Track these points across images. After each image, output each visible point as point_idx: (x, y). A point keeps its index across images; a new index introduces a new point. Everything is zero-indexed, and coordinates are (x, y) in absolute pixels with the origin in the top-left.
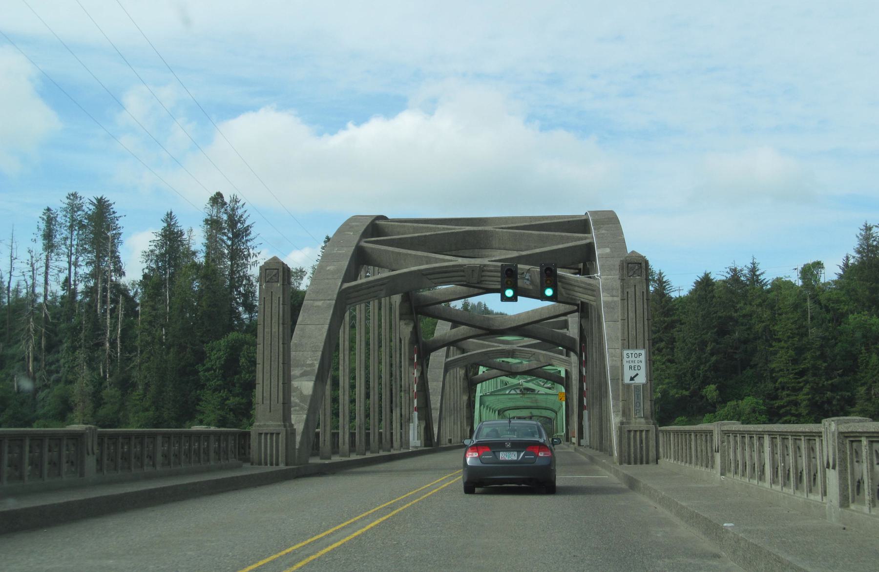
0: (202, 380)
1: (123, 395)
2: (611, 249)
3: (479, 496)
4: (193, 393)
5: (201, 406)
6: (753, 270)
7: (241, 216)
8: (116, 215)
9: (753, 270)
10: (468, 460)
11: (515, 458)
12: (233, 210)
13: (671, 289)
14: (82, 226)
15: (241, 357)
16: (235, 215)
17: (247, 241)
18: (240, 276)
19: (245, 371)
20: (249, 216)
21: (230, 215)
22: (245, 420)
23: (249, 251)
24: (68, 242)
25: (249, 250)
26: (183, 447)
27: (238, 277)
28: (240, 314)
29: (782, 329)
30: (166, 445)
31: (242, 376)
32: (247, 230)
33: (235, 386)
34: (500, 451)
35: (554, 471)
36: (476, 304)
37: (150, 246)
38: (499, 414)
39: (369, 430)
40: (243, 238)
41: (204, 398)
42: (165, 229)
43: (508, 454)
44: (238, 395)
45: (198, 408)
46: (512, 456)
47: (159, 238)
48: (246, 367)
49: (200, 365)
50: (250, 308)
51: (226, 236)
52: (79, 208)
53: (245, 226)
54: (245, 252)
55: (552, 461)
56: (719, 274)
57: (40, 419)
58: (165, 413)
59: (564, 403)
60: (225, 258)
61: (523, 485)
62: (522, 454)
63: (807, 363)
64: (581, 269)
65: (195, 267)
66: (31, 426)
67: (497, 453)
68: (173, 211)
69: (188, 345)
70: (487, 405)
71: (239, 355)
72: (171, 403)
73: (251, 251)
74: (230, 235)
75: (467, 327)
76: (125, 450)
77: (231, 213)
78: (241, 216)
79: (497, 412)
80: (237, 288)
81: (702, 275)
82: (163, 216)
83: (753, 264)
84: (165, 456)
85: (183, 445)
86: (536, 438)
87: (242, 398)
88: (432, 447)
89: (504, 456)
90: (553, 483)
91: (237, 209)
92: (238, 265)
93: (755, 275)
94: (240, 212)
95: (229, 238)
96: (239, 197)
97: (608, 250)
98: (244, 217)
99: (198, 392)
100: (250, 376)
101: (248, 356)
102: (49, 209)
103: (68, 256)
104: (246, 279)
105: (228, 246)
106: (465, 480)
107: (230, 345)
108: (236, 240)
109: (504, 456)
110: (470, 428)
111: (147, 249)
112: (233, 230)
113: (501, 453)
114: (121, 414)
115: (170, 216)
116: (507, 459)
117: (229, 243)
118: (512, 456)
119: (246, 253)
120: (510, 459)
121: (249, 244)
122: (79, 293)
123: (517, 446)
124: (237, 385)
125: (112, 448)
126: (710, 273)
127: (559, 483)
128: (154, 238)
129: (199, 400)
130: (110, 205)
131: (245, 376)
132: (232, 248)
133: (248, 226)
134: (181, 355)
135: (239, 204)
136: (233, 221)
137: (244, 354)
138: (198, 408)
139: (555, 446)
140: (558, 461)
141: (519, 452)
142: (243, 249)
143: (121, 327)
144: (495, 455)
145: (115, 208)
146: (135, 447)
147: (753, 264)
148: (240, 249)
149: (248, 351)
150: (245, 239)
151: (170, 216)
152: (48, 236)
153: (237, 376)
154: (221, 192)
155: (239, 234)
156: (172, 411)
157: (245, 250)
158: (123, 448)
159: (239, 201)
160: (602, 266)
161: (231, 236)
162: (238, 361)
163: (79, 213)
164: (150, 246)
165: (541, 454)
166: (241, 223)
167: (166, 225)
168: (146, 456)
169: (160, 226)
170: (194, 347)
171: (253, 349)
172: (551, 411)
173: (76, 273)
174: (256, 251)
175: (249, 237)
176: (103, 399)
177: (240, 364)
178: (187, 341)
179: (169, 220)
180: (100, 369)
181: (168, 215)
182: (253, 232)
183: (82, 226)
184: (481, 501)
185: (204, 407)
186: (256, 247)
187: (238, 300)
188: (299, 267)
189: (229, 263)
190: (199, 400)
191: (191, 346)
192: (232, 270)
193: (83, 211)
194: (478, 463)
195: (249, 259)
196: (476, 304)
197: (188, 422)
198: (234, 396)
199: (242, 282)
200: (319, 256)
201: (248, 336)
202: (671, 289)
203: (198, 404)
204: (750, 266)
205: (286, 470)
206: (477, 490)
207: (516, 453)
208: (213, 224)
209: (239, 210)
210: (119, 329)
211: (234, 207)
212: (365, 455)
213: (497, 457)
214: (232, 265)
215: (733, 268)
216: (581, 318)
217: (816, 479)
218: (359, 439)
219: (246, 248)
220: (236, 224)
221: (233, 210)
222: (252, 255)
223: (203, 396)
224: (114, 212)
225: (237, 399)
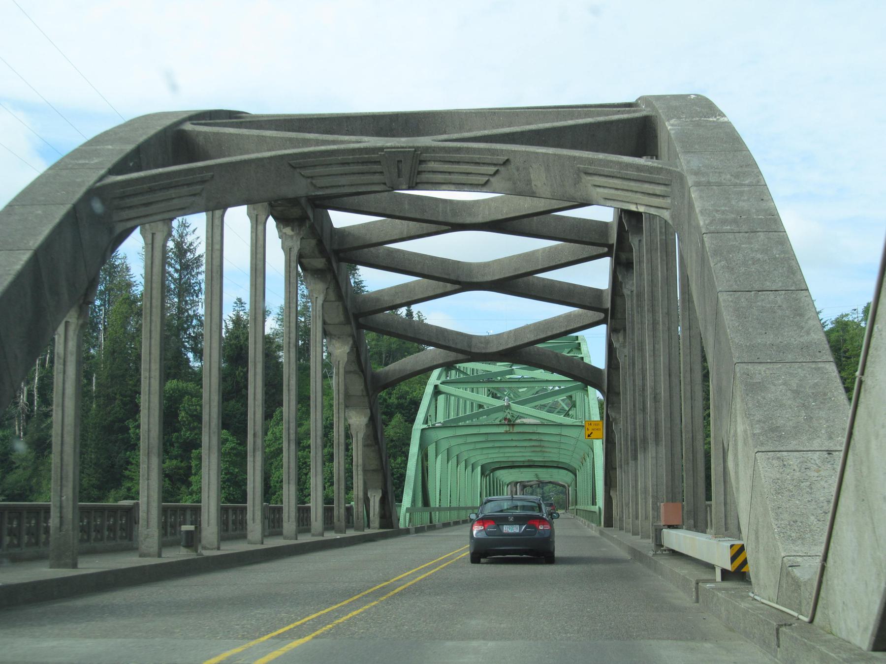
0: (132, 438)
1: (37, 458)
3: (485, 565)
4: (122, 455)
5: (130, 471)
7: (191, 244)
10: (475, 532)
11: (517, 531)
12: (181, 236)
15: (180, 410)
16: (183, 242)
18: (189, 315)
19: (185, 428)
20: (200, 243)
21: (178, 242)
22: (183, 488)
23: (200, 286)
26: (169, 520)
27: (187, 317)
28: (188, 360)
29: (850, 376)
30: (173, 517)
31: (182, 433)
33: (174, 447)
34: (503, 525)
35: (553, 542)
38: (483, 474)
40: (194, 271)
41: (134, 462)
43: (510, 527)
44: (176, 458)
45: (127, 473)
46: (515, 529)
48: (187, 422)
49: (131, 420)
50: (199, 354)
51: (172, 267)
53: (197, 255)
54: (195, 286)
55: (552, 531)
58: (85, 479)
59: (599, 447)
61: (524, 556)
62: (524, 527)
64: (613, 244)
65: (127, 301)
66: (179, 502)
67: (501, 526)
69: (118, 396)
70: (472, 462)
71: (178, 408)
72: (93, 466)
74: (178, 267)
75: (442, 350)
76: (15, 526)
77: (179, 240)
78: (191, 244)
79: (479, 469)
80: (185, 330)
84: (234, 523)
85: (42, 519)
86: (536, 513)
87: (181, 462)
88: (392, 528)
89: (507, 529)
90: (552, 553)
91: (186, 235)
92: (186, 302)
95: (176, 271)
99: (128, 453)
100: (191, 434)
101: (190, 410)
104: (197, 319)
105: (175, 280)
106: (472, 551)
107: (167, 395)
109: (507, 529)
110: (381, 495)
112: (181, 261)
113: (504, 526)
114: (34, 481)
116: (510, 531)
117: (176, 275)
118: (515, 529)
119: (196, 288)
120: (513, 531)
123: (518, 520)
124: (176, 445)
125: (85, 521)
127: (558, 553)
129: (128, 463)
131: (186, 434)
132: (180, 282)
133: (199, 256)
134: (109, 408)
137: (184, 407)
138: (127, 473)
139: (554, 520)
140: (556, 534)
141: (521, 525)
142: (193, 283)
144: (500, 529)
146: (171, 518)
148: (190, 283)
149: (190, 403)
153: (176, 434)
156: (94, 477)
157: (195, 285)
158: (95, 521)
159: (188, 226)
161: (179, 268)
162: (177, 415)
165: (541, 527)
166: (191, 252)
168: (93, 530)
170: (124, 399)
171: (196, 401)
172: (566, 472)
176: (14, 463)
177: (180, 418)
178: (116, 391)
180: (15, 426)
184: (487, 571)
185: (134, 472)
187: (186, 344)
189: (176, 300)
190: (128, 463)
191: (121, 398)
192: (179, 308)
194: (483, 535)
195: (200, 295)
197: (113, 490)
198: (171, 459)
199: (192, 322)
201: (191, 386)
203: (126, 469)
205: (198, 558)
206: (482, 560)
207: (518, 526)
209: (188, 237)
210: (37, 378)
212: (364, 531)
213: (501, 531)
216: (613, 332)
218: (339, 512)
219: (197, 283)
220: (186, 252)
223: (133, 458)
225: (174, 462)
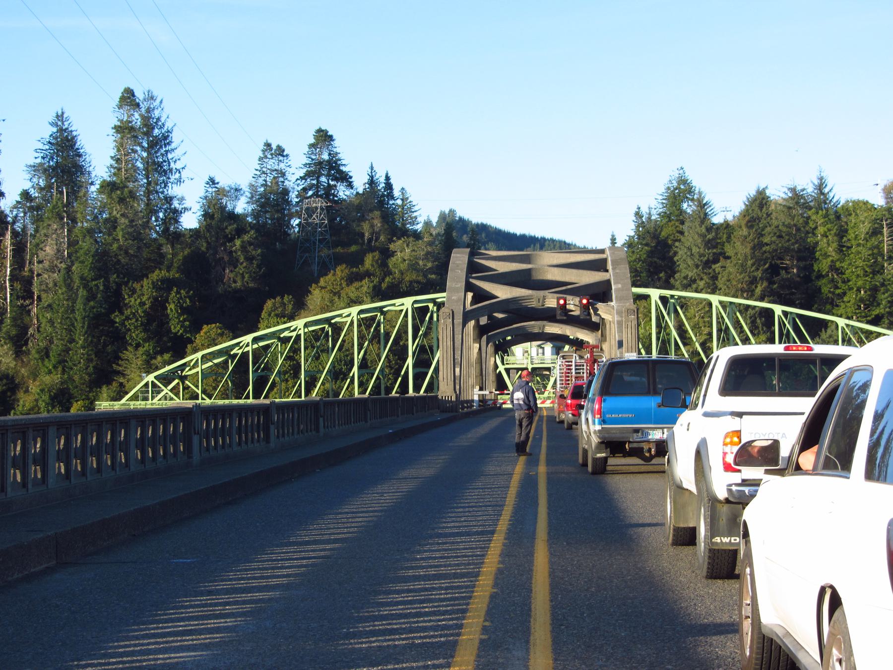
2: (622, 284)
6: (820, 187)
9: (820, 187)
13: (713, 213)
17: (167, 152)
25: (169, 163)
36: (447, 212)
37: (36, 158)
47: (47, 147)
56: (777, 193)
60: (139, 174)
63: (465, 407)
68: (65, 110)
73: (172, 165)
81: (753, 193)
82: (51, 117)
83: (821, 179)
91: (154, 109)
93: (822, 193)
96: (155, 94)
97: (620, 286)
98: (163, 120)
111: (32, 161)
115: (60, 117)
119: (165, 168)
121: (170, 156)
126: (767, 187)
128: (41, 146)
135: (157, 103)
136: (149, 124)
143: (10, 266)
147: (821, 179)
151: (60, 117)
154: (132, 88)
155: (157, 143)
160: (616, 297)
164: (36, 158)
169: (48, 131)
174: (179, 165)
175: (170, 147)
179: (60, 123)
181: (57, 116)
182: (176, 137)
186: (179, 159)
188: (234, 184)
196: (447, 212)
200: (257, 170)
202: (713, 213)
204: (816, 182)
208: (124, 129)
211: (149, 108)
215: (792, 187)
221: (149, 110)
222: (174, 170)
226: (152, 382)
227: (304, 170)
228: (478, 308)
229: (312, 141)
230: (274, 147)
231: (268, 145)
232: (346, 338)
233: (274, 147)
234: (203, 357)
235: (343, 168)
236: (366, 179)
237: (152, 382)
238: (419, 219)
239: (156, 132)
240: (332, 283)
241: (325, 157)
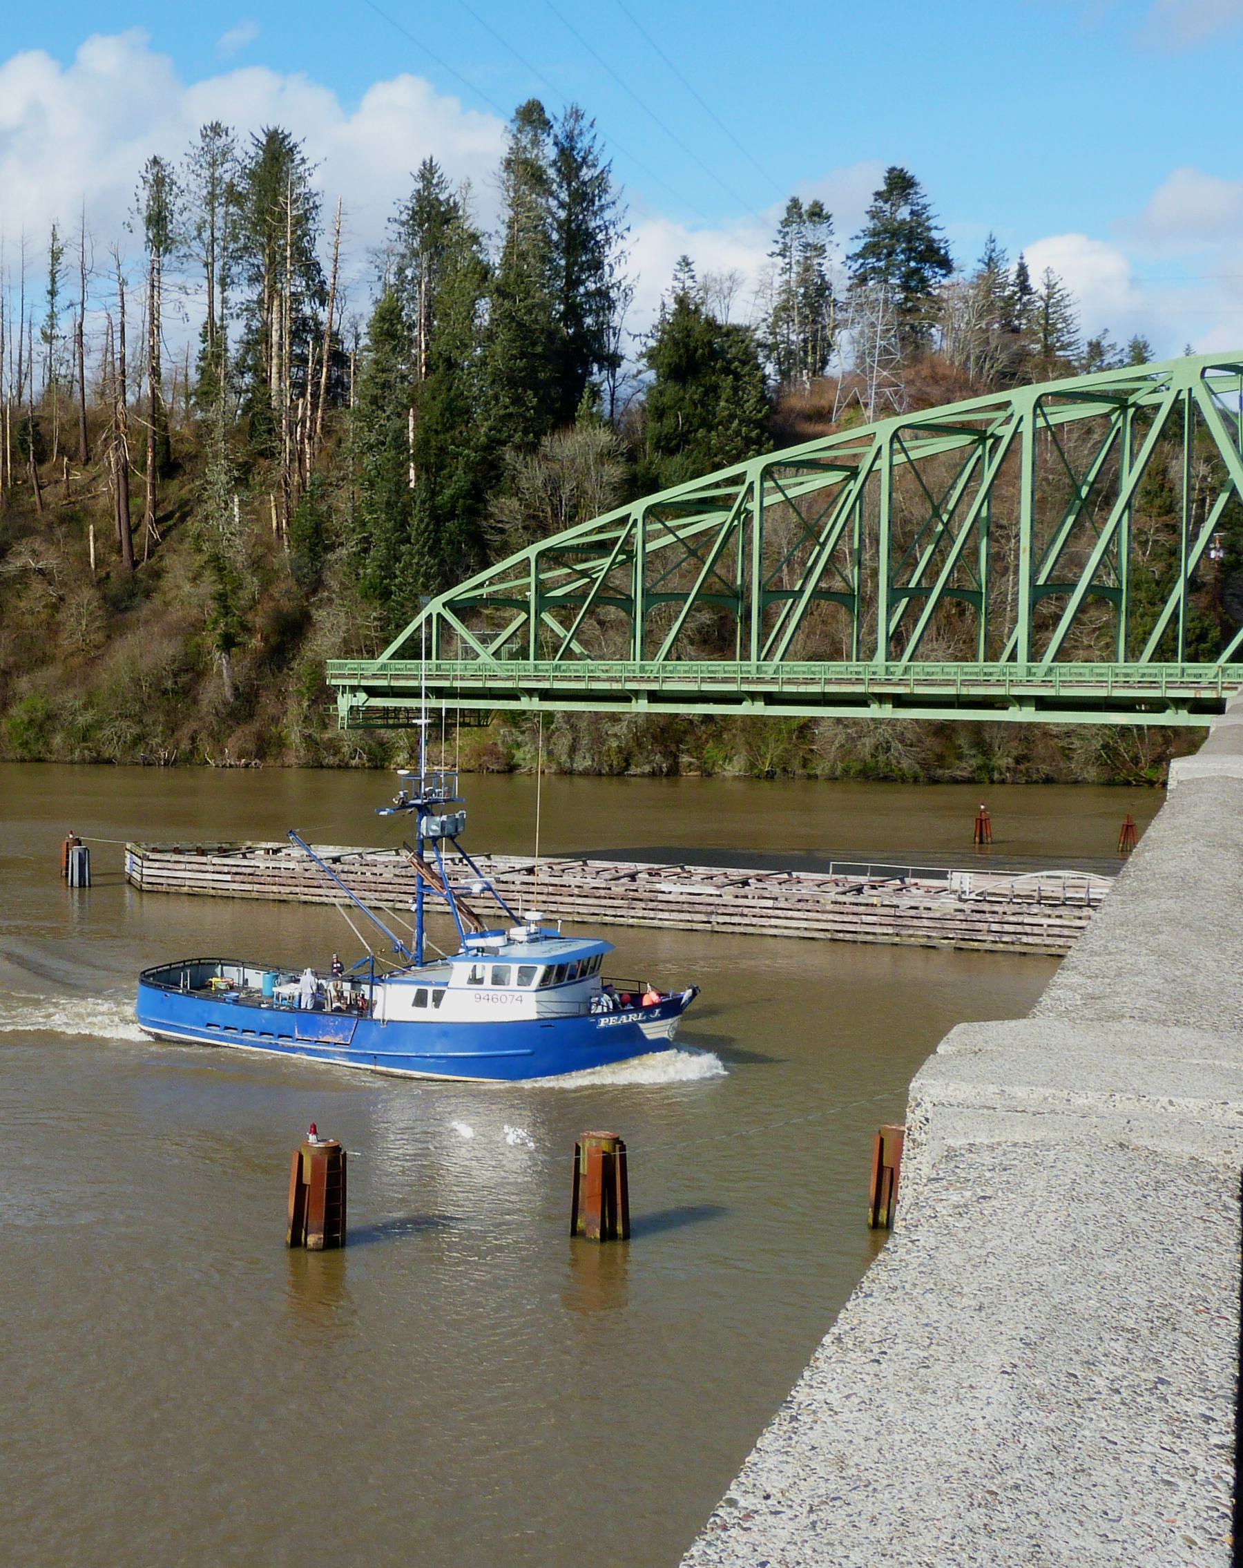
8: (309, 164)
14: (234, 197)
17: (602, 208)
24: (206, 235)
32: (601, 182)
39: (437, 659)
42: (419, 197)
52: (225, 152)
57: (314, 702)
74: (564, 196)
82: (417, 168)
91: (581, 134)
94: (583, 143)
95: (562, 205)
96: (582, 107)
102: (155, 162)
103: (206, 265)
108: (578, 209)
112: (569, 185)
117: (562, 214)
122: (785, 495)
130: (286, 137)
135: (585, 123)
136: (570, 162)
145: (304, 150)
150: (597, 203)
152: (158, 220)
161: (567, 199)
163: (227, 166)
167: (420, 185)
173: (225, 301)
182: (613, 180)
183: (234, 197)
193: (235, 160)
214: (568, 267)
217: (886, 786)
221: (570, 137)
224: (303, 161)
226: (439, 615)
227: (862, 243)
228: (616, 1204)
229: (883, 187)
230: (805, 207)
231: (795, 204)
232: (897, 496)
233: (805, 207)
234: (541, 555)
235: (935, 234)
236: (981, 253)
237: (439, 615)
238: (1081, 342)
239: (586, 174)
240: (1230, 1152)
241: (904, 213)
